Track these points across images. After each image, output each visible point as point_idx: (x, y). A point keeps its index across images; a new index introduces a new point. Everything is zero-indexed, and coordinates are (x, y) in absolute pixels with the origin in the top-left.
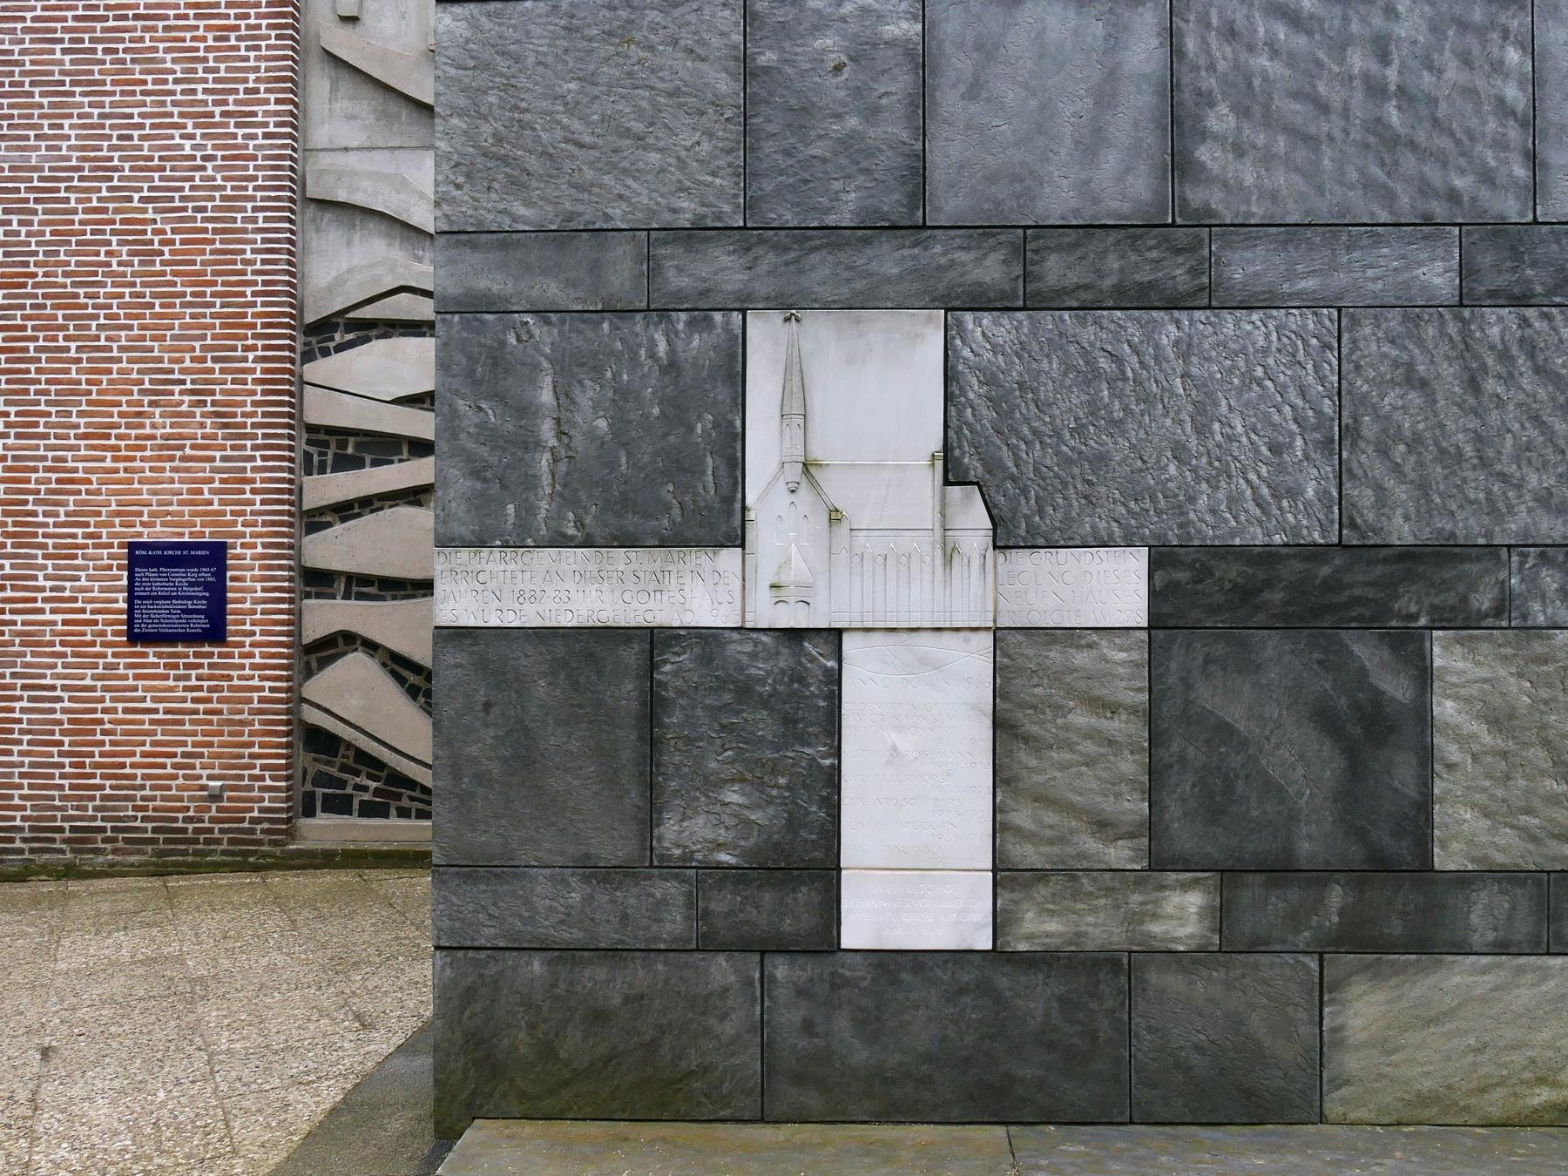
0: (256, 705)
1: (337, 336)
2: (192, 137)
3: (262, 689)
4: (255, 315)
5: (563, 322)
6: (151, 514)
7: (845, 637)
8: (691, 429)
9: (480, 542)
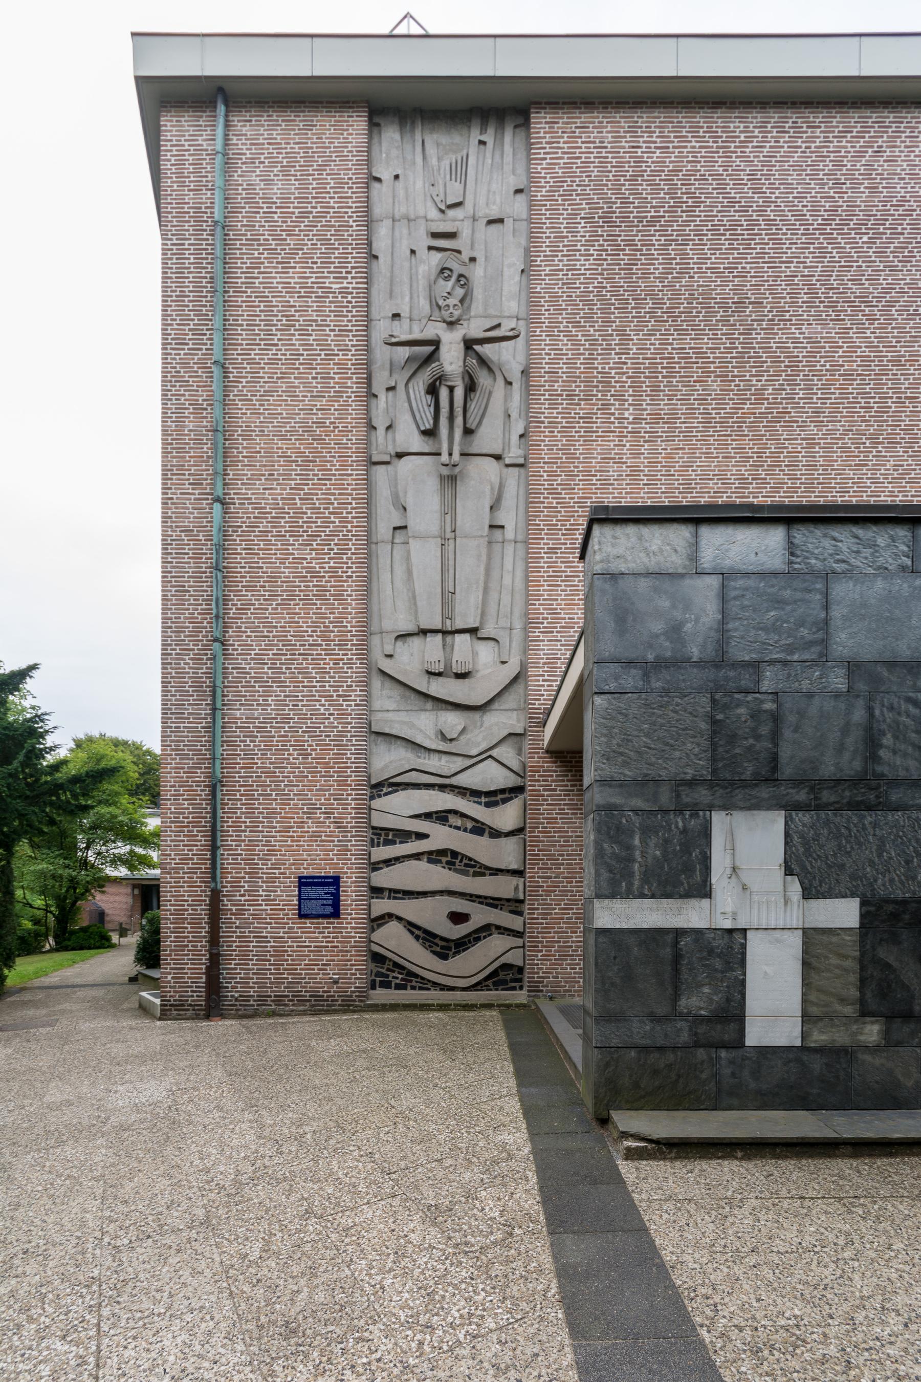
0: (353, 944)
1: (385, 789)
2: (324, 705)
3: (355, 937)
4: (351, 781)
5: (643, 815)
6: (308, 864)
7: (748, 932)
8: (691, 855)
9: (613, 896)
